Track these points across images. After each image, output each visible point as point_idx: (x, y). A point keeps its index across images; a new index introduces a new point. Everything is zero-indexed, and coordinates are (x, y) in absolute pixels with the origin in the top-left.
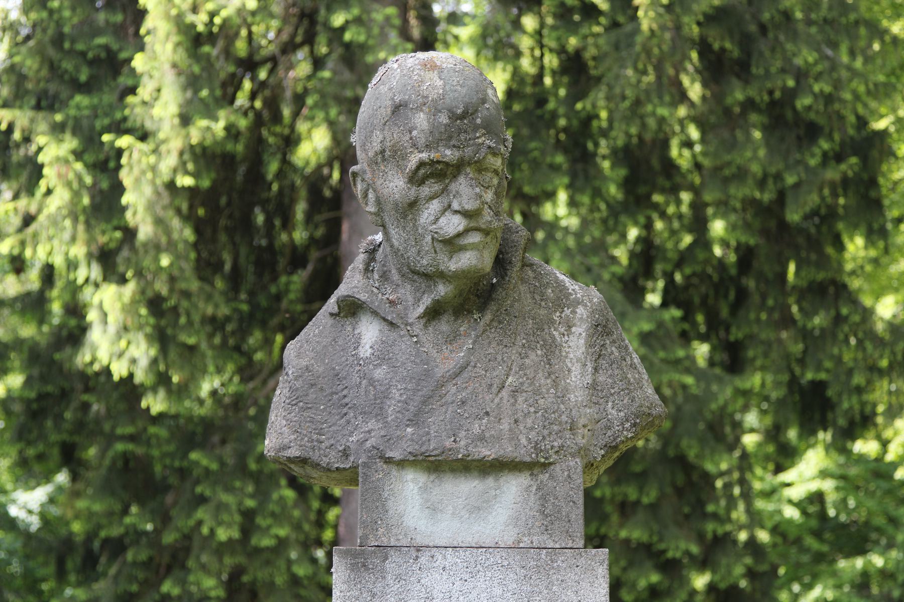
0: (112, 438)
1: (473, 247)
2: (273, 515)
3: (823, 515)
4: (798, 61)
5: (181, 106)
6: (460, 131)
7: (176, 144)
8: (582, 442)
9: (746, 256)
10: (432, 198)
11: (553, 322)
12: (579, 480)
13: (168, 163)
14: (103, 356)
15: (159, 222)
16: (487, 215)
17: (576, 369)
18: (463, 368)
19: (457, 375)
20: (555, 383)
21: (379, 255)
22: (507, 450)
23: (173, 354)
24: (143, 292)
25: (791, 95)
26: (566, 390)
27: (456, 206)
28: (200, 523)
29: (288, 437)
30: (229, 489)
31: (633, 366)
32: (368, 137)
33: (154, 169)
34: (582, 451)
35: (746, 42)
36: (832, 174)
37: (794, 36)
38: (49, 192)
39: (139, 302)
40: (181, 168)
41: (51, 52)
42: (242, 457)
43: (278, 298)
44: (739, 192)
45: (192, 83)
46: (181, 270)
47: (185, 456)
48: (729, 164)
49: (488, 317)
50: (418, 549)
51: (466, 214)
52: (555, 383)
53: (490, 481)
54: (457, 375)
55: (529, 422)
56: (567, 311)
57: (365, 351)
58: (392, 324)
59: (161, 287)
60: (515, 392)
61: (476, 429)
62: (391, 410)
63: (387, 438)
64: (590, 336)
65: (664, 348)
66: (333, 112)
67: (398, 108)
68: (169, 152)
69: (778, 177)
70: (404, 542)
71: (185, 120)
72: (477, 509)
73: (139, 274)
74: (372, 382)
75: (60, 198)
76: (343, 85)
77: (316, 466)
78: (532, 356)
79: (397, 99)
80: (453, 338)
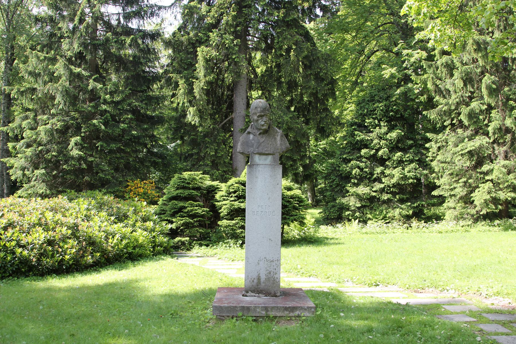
0: (190, 135)
4: (320, 66)
7: (204, 81)
9: (310, 102)
14: (190, 120)
15: (200, 95)
22: (269, 152)
23: (203, 120)
25: (319, 73)
28: (207, 151)
32: (252, 110)
33: (199, 85)
34: (279, 152)
35: (311, 62)
36: (326, 88)
37: (320, 61)
38: (180, 89)
41: (180, 63)
43: (221, 109)
45: (206, 69)
47: (204, 139)
57: (251, 139)
59: (201, 108)
62: (254, 147)
66: (233, 74)
67: (256, 108)
69: (316, 88)
71: (205, 76)
72: (265, 160)
73: (197, 105)
75: (182, 91)
76: (234, 69)
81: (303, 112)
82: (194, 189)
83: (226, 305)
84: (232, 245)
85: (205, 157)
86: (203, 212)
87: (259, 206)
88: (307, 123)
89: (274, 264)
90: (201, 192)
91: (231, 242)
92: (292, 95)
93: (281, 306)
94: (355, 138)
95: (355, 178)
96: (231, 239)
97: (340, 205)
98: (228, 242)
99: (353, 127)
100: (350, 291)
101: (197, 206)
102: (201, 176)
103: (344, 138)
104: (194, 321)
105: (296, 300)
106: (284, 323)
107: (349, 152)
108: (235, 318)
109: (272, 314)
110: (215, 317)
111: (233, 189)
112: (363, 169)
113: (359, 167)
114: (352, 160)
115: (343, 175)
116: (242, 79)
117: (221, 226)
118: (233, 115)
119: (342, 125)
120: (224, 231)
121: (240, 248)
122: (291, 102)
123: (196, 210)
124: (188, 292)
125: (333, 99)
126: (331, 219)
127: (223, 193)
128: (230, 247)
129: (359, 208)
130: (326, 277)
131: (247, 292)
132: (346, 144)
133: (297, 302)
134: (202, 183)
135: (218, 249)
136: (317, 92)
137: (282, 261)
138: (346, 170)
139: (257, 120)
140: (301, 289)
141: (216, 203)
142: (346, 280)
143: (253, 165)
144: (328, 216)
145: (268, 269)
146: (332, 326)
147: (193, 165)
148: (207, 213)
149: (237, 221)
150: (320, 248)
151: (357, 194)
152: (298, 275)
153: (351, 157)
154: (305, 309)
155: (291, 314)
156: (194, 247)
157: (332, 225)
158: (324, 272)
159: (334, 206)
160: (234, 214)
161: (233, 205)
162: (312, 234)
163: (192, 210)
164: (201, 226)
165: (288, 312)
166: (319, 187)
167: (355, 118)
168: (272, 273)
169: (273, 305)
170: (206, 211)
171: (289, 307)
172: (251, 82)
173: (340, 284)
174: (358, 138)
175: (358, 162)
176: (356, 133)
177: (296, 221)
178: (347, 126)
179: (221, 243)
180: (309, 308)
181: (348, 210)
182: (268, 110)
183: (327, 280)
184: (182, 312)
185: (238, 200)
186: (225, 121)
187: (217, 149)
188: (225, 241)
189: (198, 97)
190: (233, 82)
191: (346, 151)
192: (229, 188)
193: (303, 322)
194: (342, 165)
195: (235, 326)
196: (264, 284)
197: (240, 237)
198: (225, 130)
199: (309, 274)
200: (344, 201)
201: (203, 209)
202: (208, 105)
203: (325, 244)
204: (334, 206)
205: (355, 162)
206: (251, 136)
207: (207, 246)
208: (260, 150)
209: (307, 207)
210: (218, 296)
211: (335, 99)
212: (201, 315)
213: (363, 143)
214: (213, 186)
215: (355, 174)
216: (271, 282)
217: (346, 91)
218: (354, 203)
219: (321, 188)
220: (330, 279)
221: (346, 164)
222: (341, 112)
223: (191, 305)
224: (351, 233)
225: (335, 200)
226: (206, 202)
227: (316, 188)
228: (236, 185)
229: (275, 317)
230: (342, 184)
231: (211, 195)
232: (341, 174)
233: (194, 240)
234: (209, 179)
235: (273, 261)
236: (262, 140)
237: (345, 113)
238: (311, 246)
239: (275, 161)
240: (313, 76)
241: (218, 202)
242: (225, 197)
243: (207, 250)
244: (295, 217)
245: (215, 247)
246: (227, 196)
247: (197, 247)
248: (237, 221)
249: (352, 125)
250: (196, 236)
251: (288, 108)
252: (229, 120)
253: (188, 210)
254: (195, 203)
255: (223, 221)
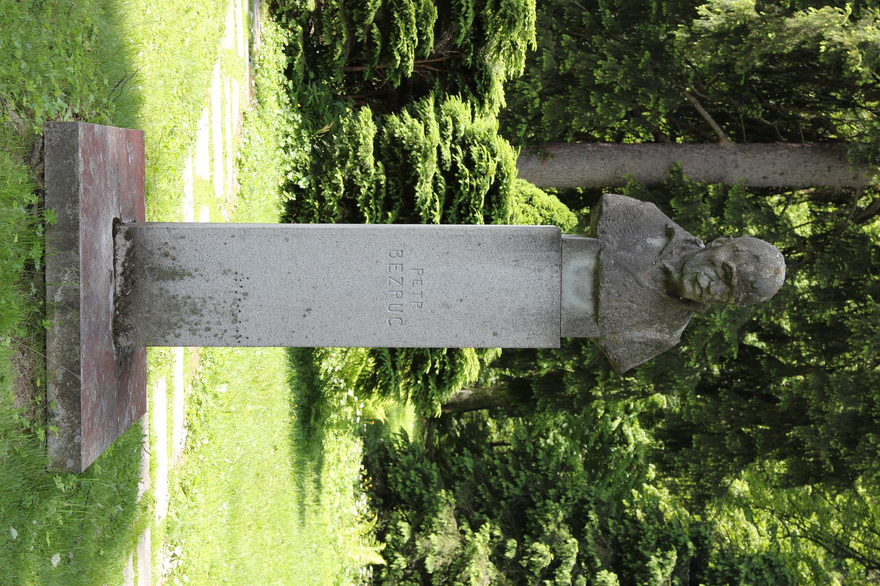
1: (694, 291)
2: (610, 104)
3: (611, 443)
5: (873, 42)
6: (746, 286)
7: (847, 41)
8: (608, 337)
10: (716, 272)
11: (662, 324)
12: (590, 336)
13: (836, 36)
15: (797, 31)
16: (708, 297)
17: (640, 334)
18: (640, 285)
19: (637, 282)
20: (633, 325)
21: (694, 246)
22: (603, 305)
24: (750, 22)
26: (631, 330)
27: (712, 283)
28: (604, 58)
29: (612, 206)
30: (626, 75)
31: (642, 359)
33: (832, 26)
34: (603, 337)
39: (745, 20)
40: (832, 43)
42: (645, 83)
43: (748, 103)
44: (811, 397)
46: (766, 45)
48: (832, 391)
49: (664, 296)
50: (561, 266)
51: (708, 288)
52: (633, 325)
53: (590, 297)
54: (637, 282)
55: (616, 314)
56: (667, 330)
57: (650, 241)
58: (661, 253)
59: (754, 33)
60: (629, 308)
61: (613, 291)
62: (622, 253)
63: (609, 252)
64: (656, 340)
65: (713, 347)
66: (868, 140)
67: (757, 258)
68: (842, 36)
69: (822, 421)
70: (563, 260)
71: (863, 46)
72: (578, 292)
73: (763, 19)
74: (635, 244)
77: (598, 219)
78: (646, 315)
79: (761, 258)
80: (654, 280)
81: (742, 374)
82: (479, 23)
83: (81, 169)
84: (293, 154)
85: (587, 50)
86: (403, 56)
87: (420, 271)
88: (706, 387)
89: (227, 324)
90: (467, 46)
91: (304, 154)
92: (798, 339)
93: (83, 355)
94: (654, 550)
95: (521, 553)
96: (314, 152)
97: (430, 502)
98: (302, 143)
99: (690, 545)
100: (140, 569)
101: (420, 34)
102: (522, 46)
103: (656, 514)
104: (24, 58)
105: (104, 403)
106: (22, 370)
107: (606, 531)
108: (35, 200)
109: (53, 325)
110: (37, 130)
111: (481, 157)
112: (551, 577)
113: (557, 563)
114: (582, 541)
115: (530, 511)
116: (851, 171)
117: (356, 117)
118: (727, 143)
119: (698, 503)
120: (339, 126)
121: (282, 182)
122: (773, 335)
123: (408, 31)
124: (128, 25)
125: (786, 476)
126: (386, 471)
127: (465, 124)
128: (286, 149)
129: (421, 565)
130: (187, 483)
131: (128, 236)
132: (634, 521)
133: (95, 406)
134: (499, 48)
135: (277, 110)
136: (807, 422)
137: (239, 351)
138: (547, 521)
139: (712, 263)
140: (142, 411)
141: (431, 101)
142: (178, 551)
143: (560, 251)
144: (395, 461)
145: (210, 305)
146: (15, 533)
147: (558, 12)
148: (397, 71)
149: (373, 171)
150: (288, 449)
151: (468, 559)
152: (194, 386)
153: (589, 537)
154: (71, 438)
155: (53, 391)
156: (284, 26)
157: (364, 477)
158: (204, 473)
159: (426, 480)
160: (396, 160)
161: (425, 157)
162: (334, 416)
163: (406, 18)
164: (356, 50)
165: (60, 378)
166: (491, 423)
167: (721, 551)
168: (194, 318)
169: (84, 329)
170: (403, 68)
171: (78, 384)
172: (843, 198)
173: (161, 534)
174: (654, 561)
175: (573, 562)
176: (673, 555)
177: (376, 368)
178: (697, 524)
179: (298, 117)
180: (76, 451)
181: (416, 529)
182: (747, 299)
183: (178, 488)
184: (55, 13)
185: (443, 173)
186: (708, 117)
187: (612, 90)
188: (304, 133)
189: (790, 22)
190: (842, 139)
191: (611, 522)
192: (483, 142)
193: (28, 431)
194: (562, 507)
195: (9, 200)
196: (156, 291)
197: (318, 182)
198: (677, 115)
199: (196, 424)
200: (445, 517)
201: (412, 56)
202: (762, 57)
203: (300, 465)
204: (426, 480)
205: (576, 550)
206: (657, 242)
207: (289, 72)
208: (610, 274)
209: (422, 400)
210: (113, 135)
211: (787, 482)
212: (46, 80)
213: (637, 577)
214: (488, 86)
215: (534, 552)
216: (165, 316)
217: (814, 518)
218: (437, 549)
219: (486, 432)
220: (181, 496)
221: (566, 521)
222: (741, 503)
223: (79, 39)
224: (340, 543)
225: (448, 486)
226: (435, 65)
227: (485, 412)
228: (493, 166)
229: (42, 337)
230: (499, 508)
231: (459, 81)
232: (533, 505)
233: (306, 27)
234: (512, 72)
235: (235, 321)
236: (645, 279)
237: (740, 514)
238: (294, 418)
239: (574, 322)
240: (866, 410)
241: (437, 105)
242: (450, 127)
243: (274, 73)
244: (388, 364)
245: (285, 99)
246: (455, 138)
247: (284, 36)
248: (373, 171)
249: (697, 539)
250: (319, 31)
251: (753, 327)
252: (711, 129)
253: (406, 7)
254: (430, 29)
255: (371, 123)
